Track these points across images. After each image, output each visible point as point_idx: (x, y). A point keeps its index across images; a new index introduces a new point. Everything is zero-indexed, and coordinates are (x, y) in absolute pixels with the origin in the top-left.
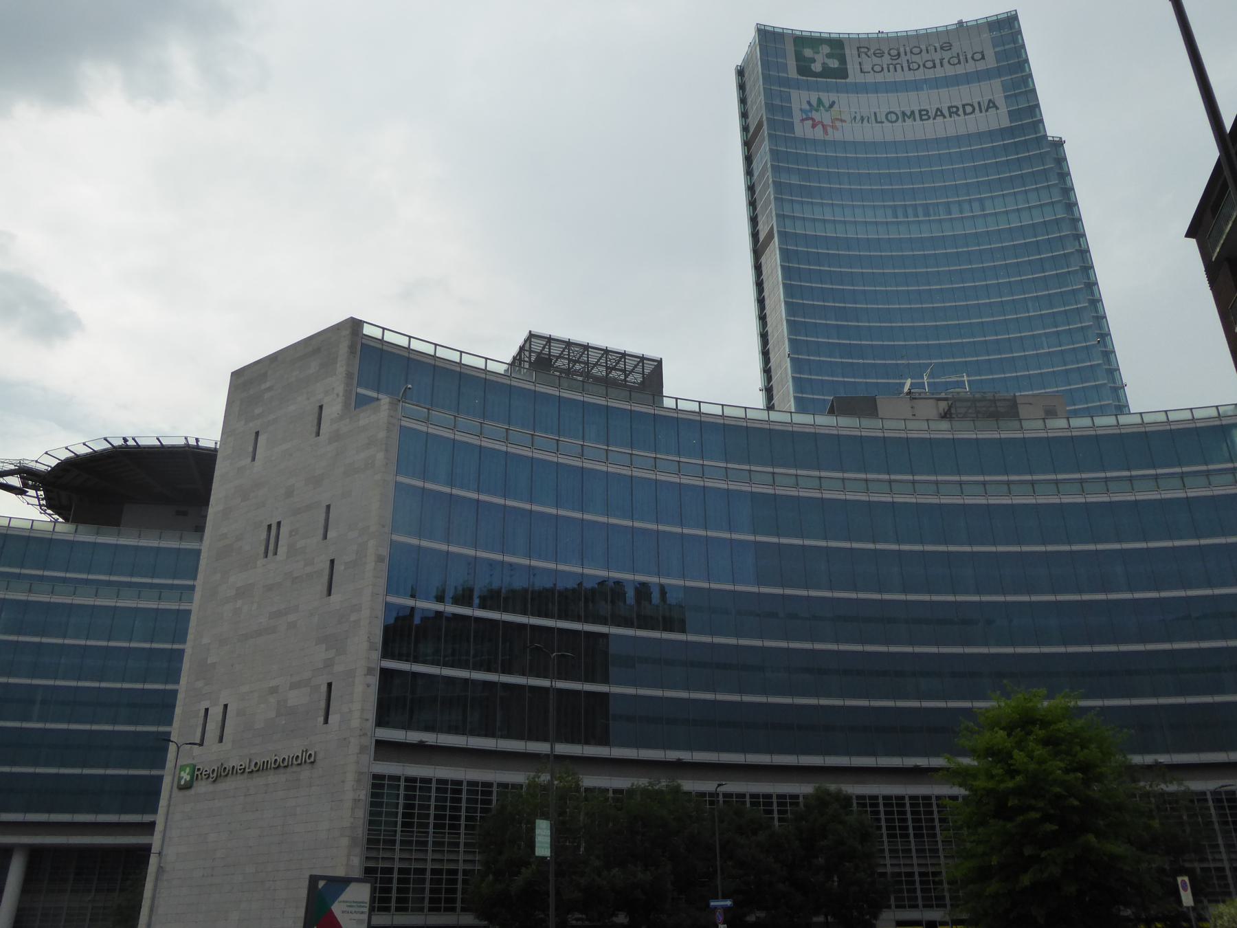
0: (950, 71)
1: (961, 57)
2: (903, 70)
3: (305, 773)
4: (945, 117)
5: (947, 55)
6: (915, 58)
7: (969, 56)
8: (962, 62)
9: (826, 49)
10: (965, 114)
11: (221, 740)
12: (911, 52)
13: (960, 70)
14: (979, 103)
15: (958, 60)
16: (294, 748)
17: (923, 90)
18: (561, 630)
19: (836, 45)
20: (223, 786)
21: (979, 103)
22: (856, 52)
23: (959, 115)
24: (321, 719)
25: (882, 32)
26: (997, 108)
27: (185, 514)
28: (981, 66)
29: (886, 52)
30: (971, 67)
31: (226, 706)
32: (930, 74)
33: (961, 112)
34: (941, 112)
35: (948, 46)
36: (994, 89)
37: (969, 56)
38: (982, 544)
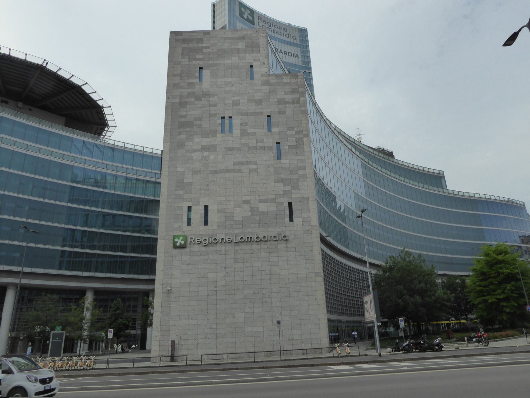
0: (286, 39)
1: (289, 36)
2: (271, 31)
3: (282, 245)
4: (283, 54)
5: (285, 33)
6: (275, 29)
7: (292, 37)
8: (289, 37)
9: (248, 12)
10: (289, 55)
11: (206, 223)
12: (274, 26)
13: (288, 40)
14: (293, 54)
15: (288, 36)
16: (271, 232)
17: (277, 41)
18: (112, 234)
19: (252, 12)
20: (211, 249)
21: (293, 54)
22: (257, 17)
23: (287, 55)
24: (288, 219)
25: (266, 15)
26: (298, 58)
27: (6, 103)
28: (295, 41)
29: (267, 22)
30: (292, 40)
31: (206, 207)
32: (279, 37)
33: (288, 54)
34: (282, 51)
35: (285, 30)
36: (297, 51)
37: (292, 37)
38: (471, 213)
